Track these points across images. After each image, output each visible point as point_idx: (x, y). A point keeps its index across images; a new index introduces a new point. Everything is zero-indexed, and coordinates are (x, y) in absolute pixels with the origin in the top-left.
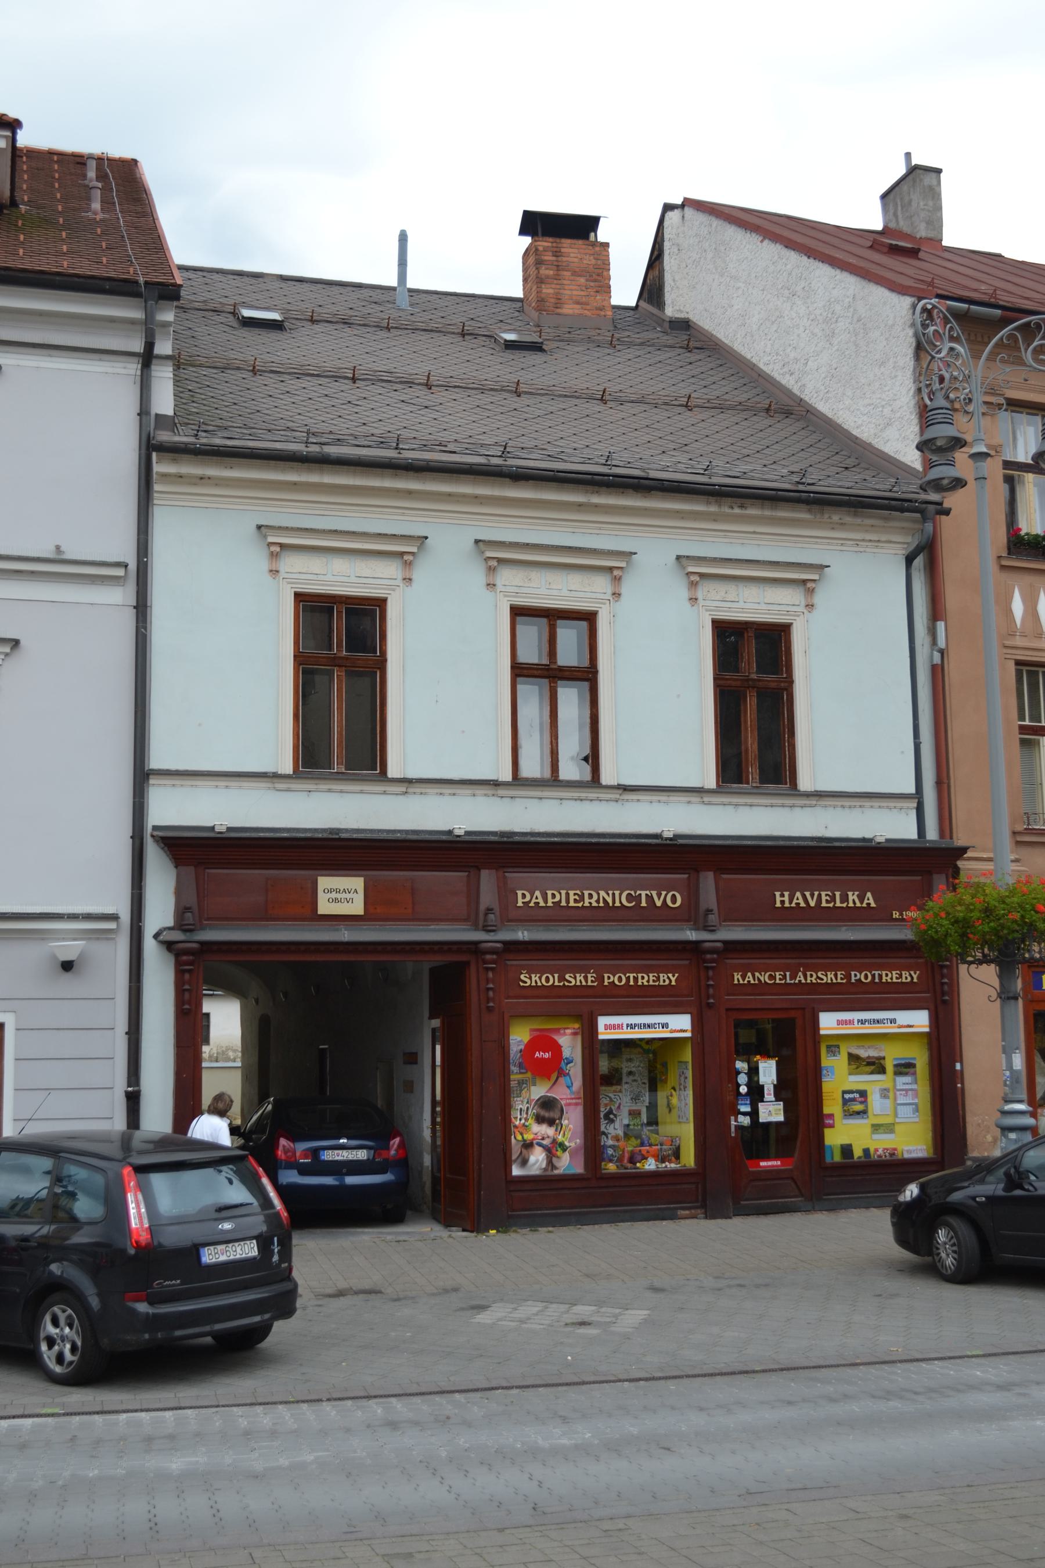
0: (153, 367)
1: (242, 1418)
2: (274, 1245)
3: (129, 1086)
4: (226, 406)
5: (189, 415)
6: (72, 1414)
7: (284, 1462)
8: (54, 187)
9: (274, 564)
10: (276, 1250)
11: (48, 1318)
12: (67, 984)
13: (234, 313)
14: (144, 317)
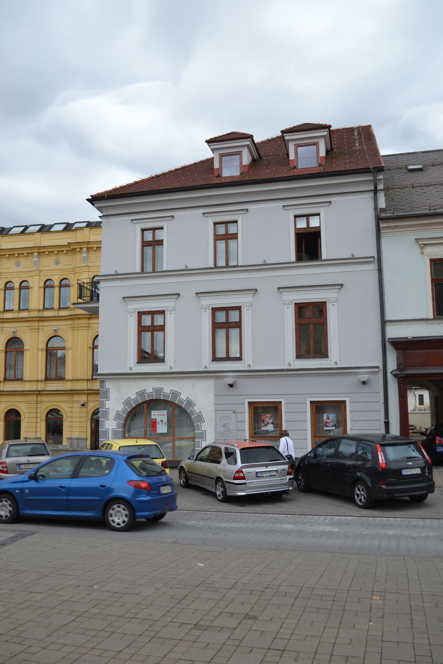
0: (378, 194)
1: (414, 522)
2: (426, 470)
3: (385, 420)
4: (404, 201)
5: (391, 206)
6: (363, 517)
7: (423, 535)
8: (344, 140)
9: (422, 251)
10: (427, 472)
11: (357, 488)
12: (364, 388)
13: (406, 168)
14: (373, 178)
